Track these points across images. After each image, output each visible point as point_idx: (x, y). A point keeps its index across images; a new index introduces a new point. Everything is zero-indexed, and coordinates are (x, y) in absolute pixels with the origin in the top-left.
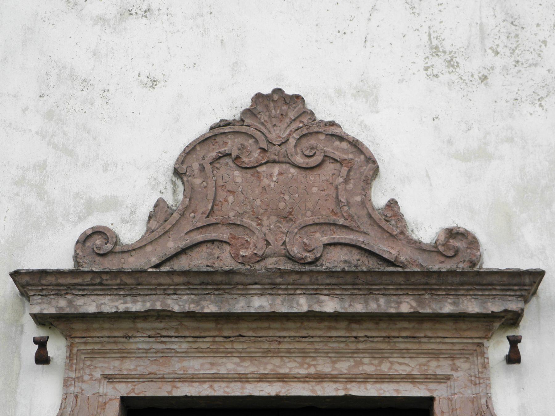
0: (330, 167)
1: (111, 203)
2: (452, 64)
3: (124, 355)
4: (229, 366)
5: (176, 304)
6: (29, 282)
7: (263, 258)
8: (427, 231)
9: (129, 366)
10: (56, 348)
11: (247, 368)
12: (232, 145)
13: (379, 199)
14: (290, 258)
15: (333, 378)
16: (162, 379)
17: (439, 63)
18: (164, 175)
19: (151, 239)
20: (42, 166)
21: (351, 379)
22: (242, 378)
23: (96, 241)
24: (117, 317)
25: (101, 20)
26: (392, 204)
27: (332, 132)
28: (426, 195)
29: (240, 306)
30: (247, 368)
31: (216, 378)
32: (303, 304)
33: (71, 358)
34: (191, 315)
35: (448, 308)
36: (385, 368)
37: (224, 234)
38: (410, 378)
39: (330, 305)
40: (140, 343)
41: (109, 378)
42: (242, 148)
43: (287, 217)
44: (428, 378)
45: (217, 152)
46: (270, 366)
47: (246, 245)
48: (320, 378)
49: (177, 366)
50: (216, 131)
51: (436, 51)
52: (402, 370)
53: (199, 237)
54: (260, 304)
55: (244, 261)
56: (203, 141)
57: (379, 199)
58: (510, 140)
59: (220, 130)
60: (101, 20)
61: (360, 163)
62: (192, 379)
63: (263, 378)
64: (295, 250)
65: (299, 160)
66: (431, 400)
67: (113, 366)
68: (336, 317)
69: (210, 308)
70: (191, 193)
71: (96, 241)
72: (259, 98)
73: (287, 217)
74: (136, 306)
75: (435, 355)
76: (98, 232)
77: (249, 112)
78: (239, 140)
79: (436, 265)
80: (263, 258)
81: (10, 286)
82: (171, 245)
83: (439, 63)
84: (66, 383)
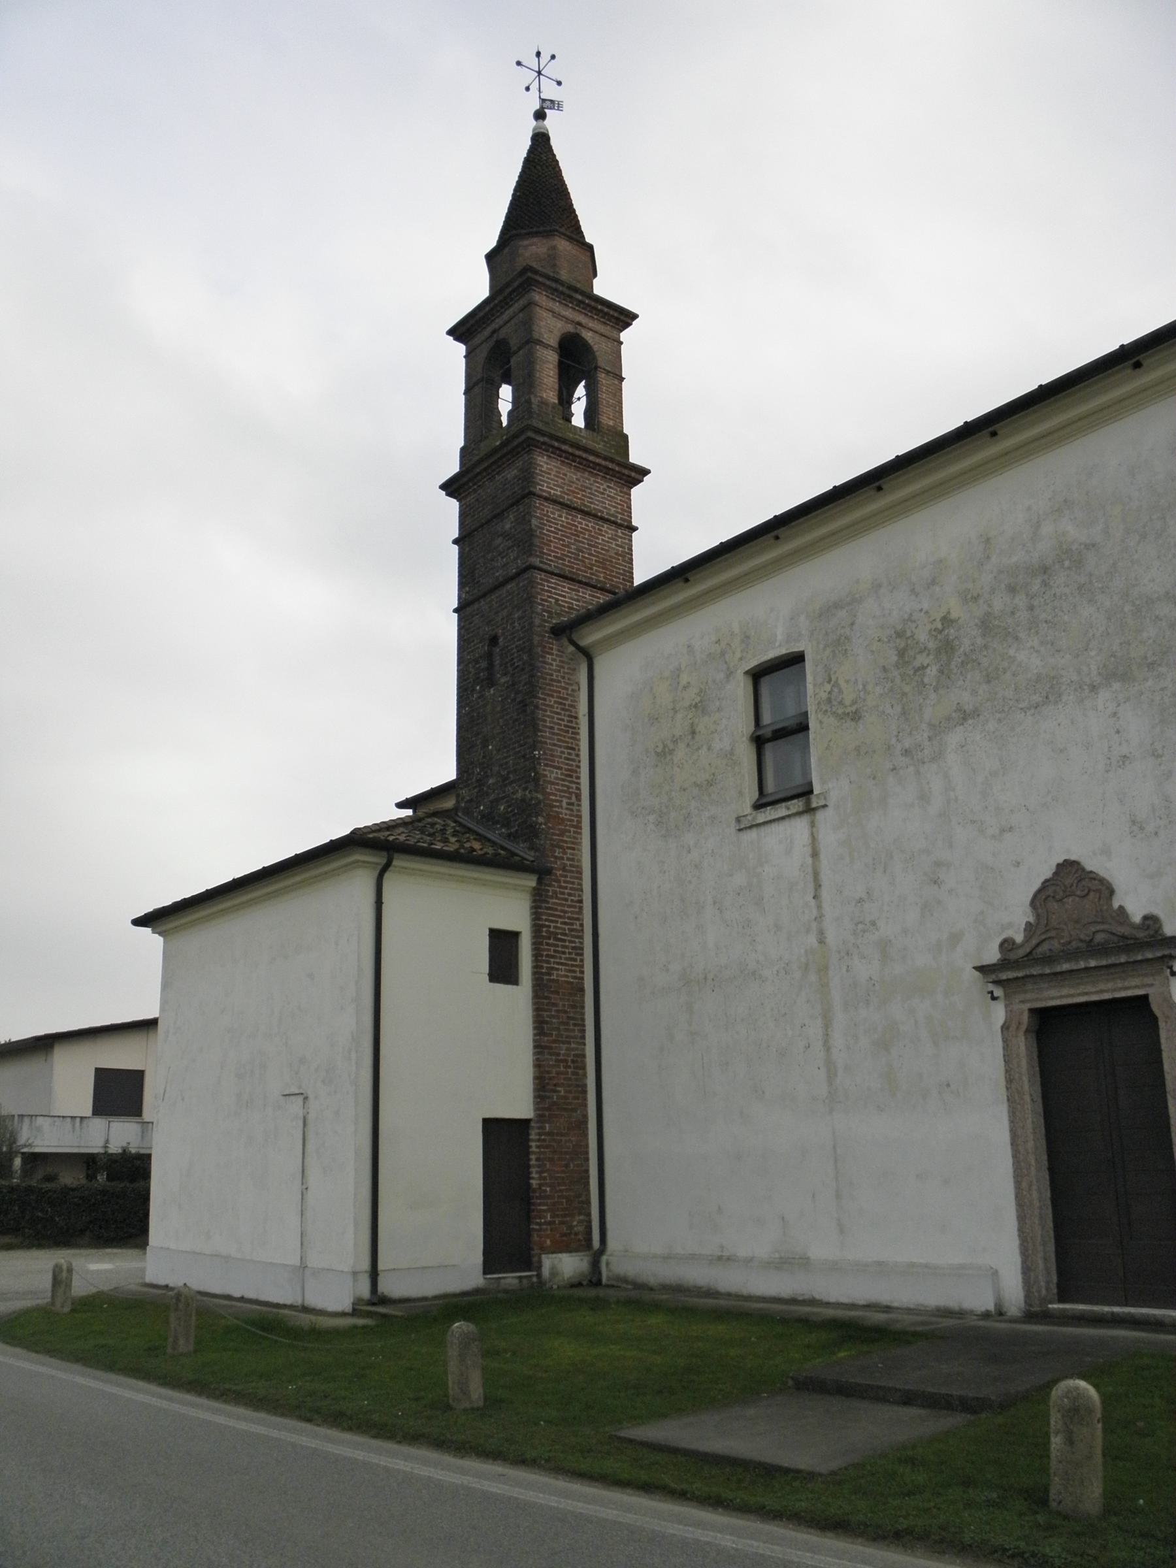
0: (1092, 894)
1: (1010, 925)
2: (1142, 828)
3: (1025, 992)
4: (1065, 992)
5: (1035, 971)
6: (981, 969)
7: (1070, 943)
8: (1137, 919)
9: (1029, 996)
10: (998, 992)
11: (1072, 991)
12: (1050, 891)
13: (1116, 905)
14: (1081, 941)
15: (1107, 991)
16: (1041, 1000)
17: (1135, 828)
18: (1029, 910)
19: (1028, 939)
20: (982, 912)
21: (1115, 990)
22: (1072, 996)
23: (1007, 945)
24: (1017, 979)
25: (993, 837)
26: (1121, 907)
27: (1092, 876)
28: (1136, 900)
29: (1058, 969)
30: (1072, 991)
31: (1061, 997)
32: (1082, 965)
33: (1006, 996)
34: (1041, 975)
35: (1139, 957)
36: (1126, 984)
37: (1053, 934)
38: (1136, 987)
39: (1093, 963)
40: (1029, 987)
41: (1022, 1002)
42: (1055, 892)
43: (1077, 922)
44: (1144, 986)
45: (1044, 897)
46: (1081, 989)
47: (1063, 937)
48: (1102, 991)
49: (1046, 994)
50: (614, 1283)
51: (1134, 822)
52: (1133, 984)
53: (1043, 937)
54: (1066, 966)
55: (1064, 945)
56: (1039, 891)
57: (1116, 905)
58: (1170, 864)
59: (1046, 884)
60: (993, 837)
61: (1106, 890)
62: (1053, 998)
63: (1079, 995)
64: (1082, 937)
65: (1078, 893)
66: (1145, 998)
67: (1022, 997)
68: (1095, 967)
69: (1048, 971)
70: (1038, 916)
71: (1007, 945)
72: (1058, 865)
73: (1077, 922)
74: (1020, 974)
75: (1146, 975)
76: (1005, 941)
77: (1055, 874)
78: (1053, 888)
79: (1141, 935)
80: (1070, 943)
81: (977, 974)
82: (1034, 942)
83: (1135, 828)
84: (1006, 1006)
